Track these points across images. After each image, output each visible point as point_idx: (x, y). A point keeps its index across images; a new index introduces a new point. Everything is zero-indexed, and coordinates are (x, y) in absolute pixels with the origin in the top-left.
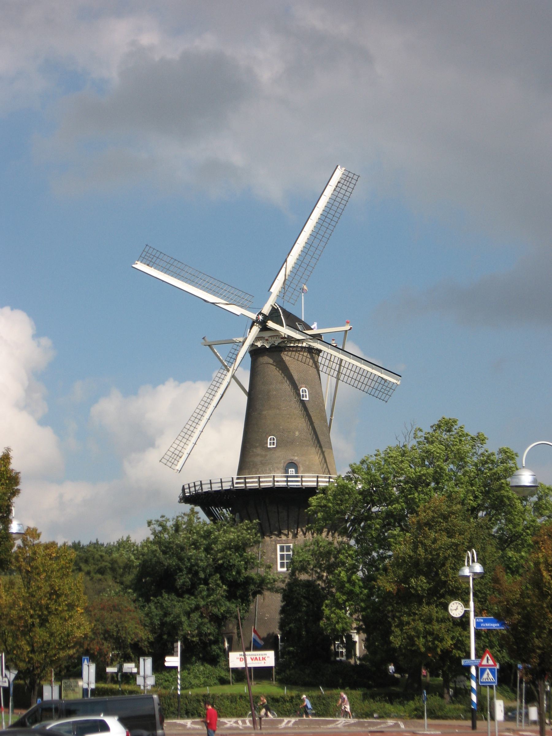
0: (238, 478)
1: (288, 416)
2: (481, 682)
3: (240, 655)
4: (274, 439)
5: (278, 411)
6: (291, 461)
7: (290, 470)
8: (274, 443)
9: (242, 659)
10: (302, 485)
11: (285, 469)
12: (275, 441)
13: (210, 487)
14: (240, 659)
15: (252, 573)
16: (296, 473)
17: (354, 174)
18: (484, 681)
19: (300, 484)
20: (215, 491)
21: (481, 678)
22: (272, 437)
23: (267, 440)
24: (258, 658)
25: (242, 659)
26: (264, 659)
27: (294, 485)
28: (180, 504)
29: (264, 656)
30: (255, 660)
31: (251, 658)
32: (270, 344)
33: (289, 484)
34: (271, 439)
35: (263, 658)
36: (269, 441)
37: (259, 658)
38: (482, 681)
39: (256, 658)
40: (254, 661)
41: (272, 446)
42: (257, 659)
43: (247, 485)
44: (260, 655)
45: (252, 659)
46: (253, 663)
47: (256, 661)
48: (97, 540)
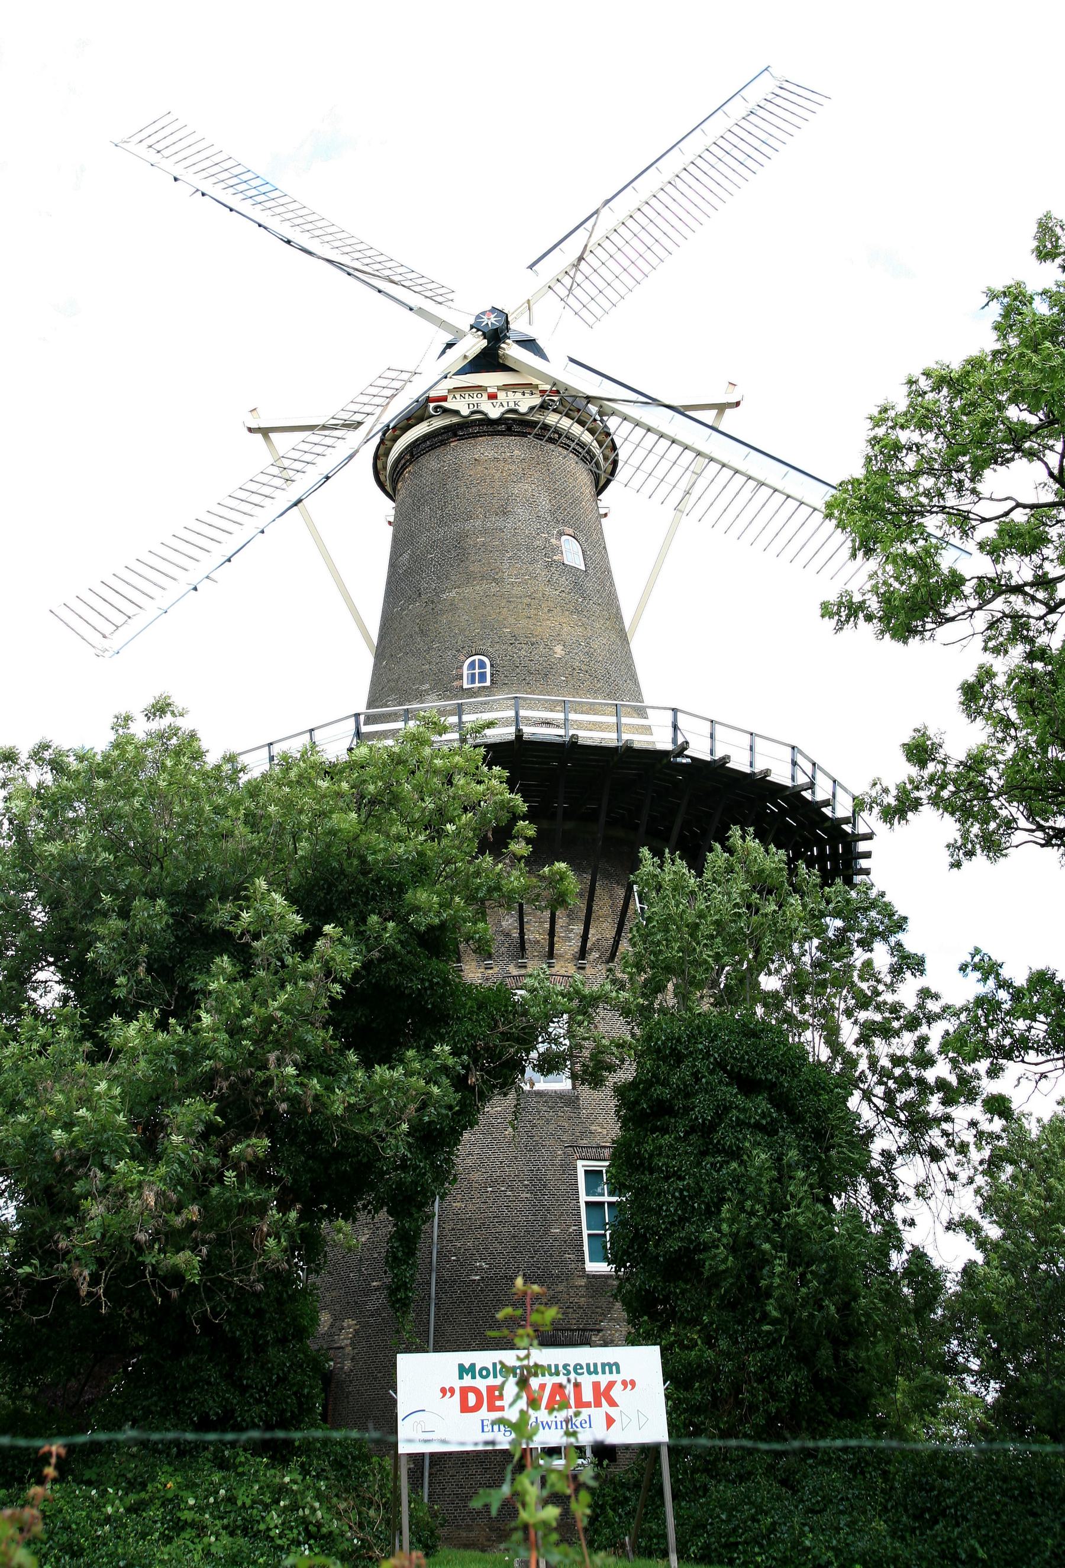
1: (527, 600)
3: (462, 1370)
4: (482, 665)
5: (494, 588)
9: (472, 1399)
12: (488, 670)
14: (464, 1391)
22: (477, 657)
23: (461, 667)
25: (472, 1399)
26: (603, 1395)
28: (1033, 229)
29: (604, 1380)
32: (502, 410)
34: (472, 665)
35: (596, 1385)
36: (465, 672)
37: (577, 1385)
44: (577, 1367)
48: (207, 751)
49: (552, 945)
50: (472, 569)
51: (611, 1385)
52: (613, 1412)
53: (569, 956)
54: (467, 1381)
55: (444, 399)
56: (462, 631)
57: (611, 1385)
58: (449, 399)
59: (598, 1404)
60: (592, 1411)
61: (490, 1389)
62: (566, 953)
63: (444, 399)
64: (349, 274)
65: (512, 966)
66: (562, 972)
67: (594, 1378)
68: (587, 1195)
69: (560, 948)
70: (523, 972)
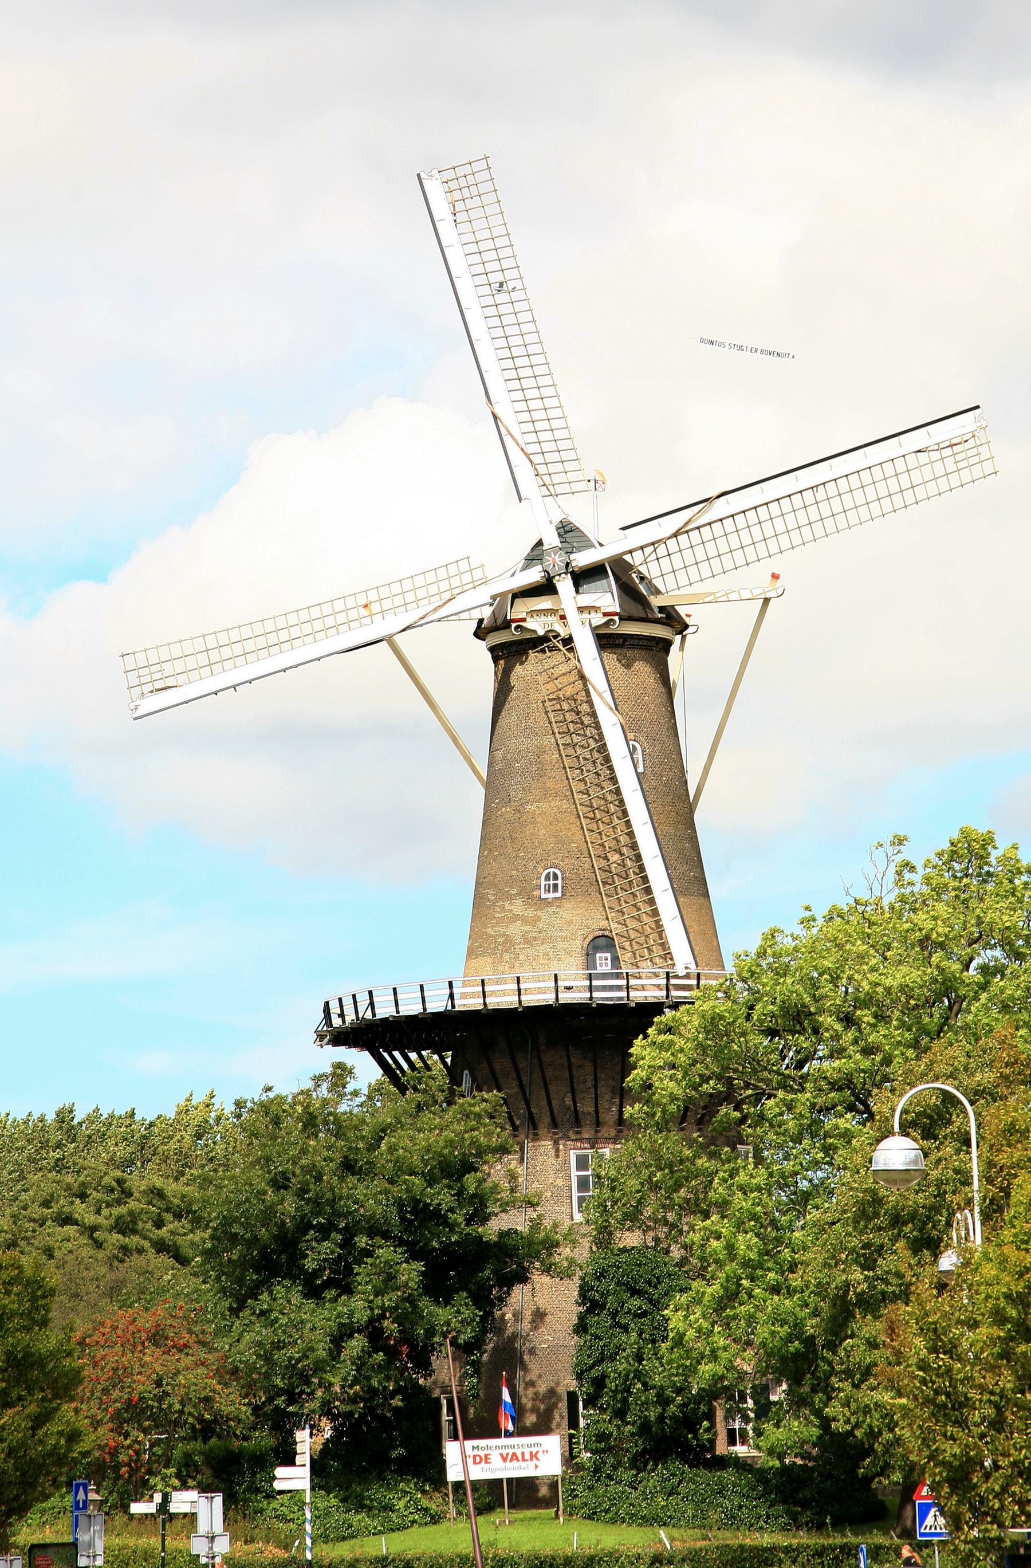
0: (465, 984)
2: (922, 1535)
6: (601, 933)
7: (598, 955)
8: (555, 886)
10: (591, 998)
11: (587, 955)
12: (559, 882)
13: (481, 990)
15: (493, 1228)
16: (614, 967)
17: (518, 267)
18: (927, 1530)
19: (624, 994)
20: (433, 1014)
21: (920, 1526)
22: (552, 870)
23: (540, 878)
24: (520, 1457)
26: (533, 1456)
27: (611, 999)
29: (534, 1450)
30: (511, 1460)
31: (501, 1455)
33: (595, 995)
34: (547, 878)
35: (531, 1453)
37: (523, 1454)
38: (922, 1531)
39: (514, 1454)
40: (508, 1464)
41: (551, 895)
42: (517, 1460)
43: (595, 995)
45: (505, 1460)
46: (505, 1469)
47: (515, 1462)
49: (597, 1117)
50: (548, 785)
51: (537, 1452)
52: (538, 1463)
53: (611, 1122)
54: (476, 1452)
55: (524, 620)
56: (541, 844)
57: (537, 1452)
58: (528, 619)
59: (531, 1459)
60: (529, 1462)
61: (486, 1456)
62: (609, 1121)
63: (524, 620)
64: (421, 625)
65: (571, 1132)
66: (606, 1135)
67: (530, 1450)
68: (448, 1416)
69: (604, 1117)
70: (579, 1137)
